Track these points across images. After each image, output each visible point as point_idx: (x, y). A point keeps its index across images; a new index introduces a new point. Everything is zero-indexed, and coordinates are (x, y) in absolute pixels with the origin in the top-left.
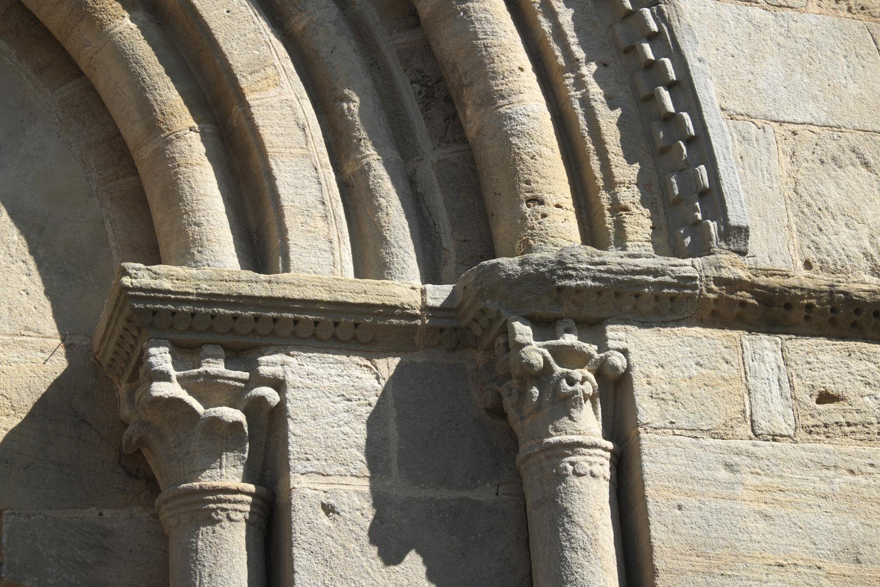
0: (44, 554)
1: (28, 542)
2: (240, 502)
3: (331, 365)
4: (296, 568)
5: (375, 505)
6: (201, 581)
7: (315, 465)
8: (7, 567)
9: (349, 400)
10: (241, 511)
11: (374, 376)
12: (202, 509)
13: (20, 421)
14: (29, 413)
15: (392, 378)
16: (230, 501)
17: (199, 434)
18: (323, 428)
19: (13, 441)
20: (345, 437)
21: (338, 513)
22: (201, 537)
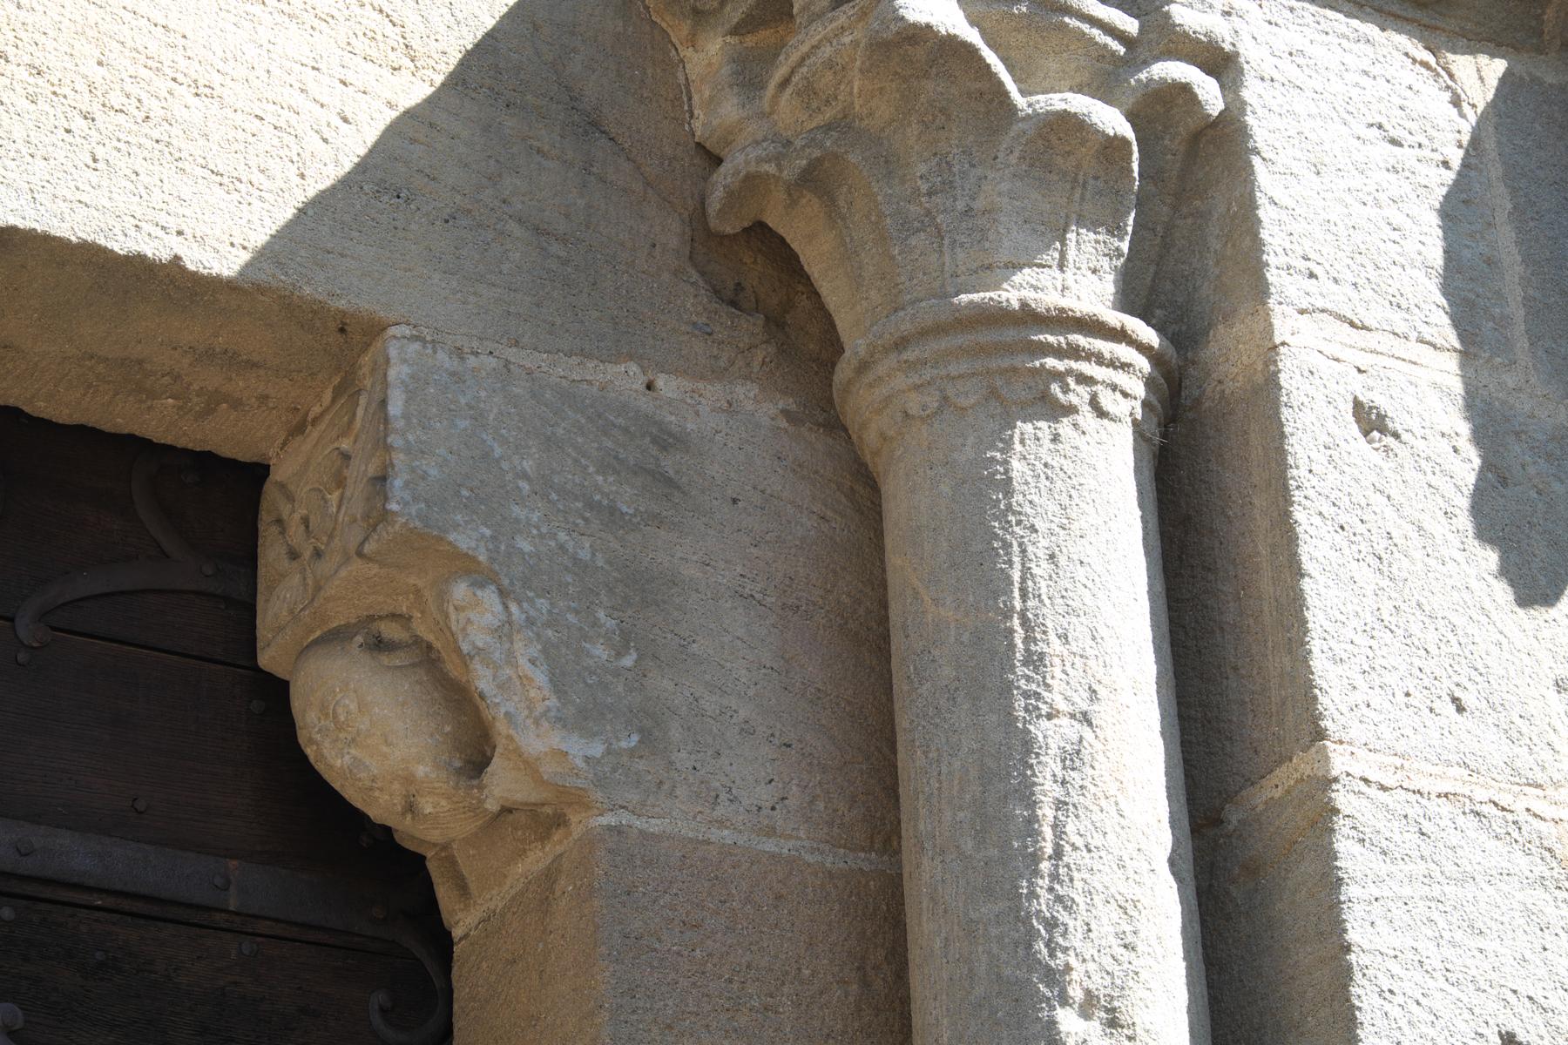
0: (505, 465)
1: (463, 424)
2: (1125, 366)
3: (1344, 43)
4: (1307, 565)
5: (1478, 438)
6: (1026, 570)
7: (1338, 297)
8: (407, 484)
9: (1394, 142)
10: (1125, 395)
11: (1447, 95)
12: (1017, 367)
13: (429, 91)
14: (451, 74)
15: (1492, 105)
16: (1099, 359)
17: (1013, 159)
18: (1341, 200)
19: (413, 141)
20: (1395, 236)
21: (1396, 436)
22: (1018, 447)
